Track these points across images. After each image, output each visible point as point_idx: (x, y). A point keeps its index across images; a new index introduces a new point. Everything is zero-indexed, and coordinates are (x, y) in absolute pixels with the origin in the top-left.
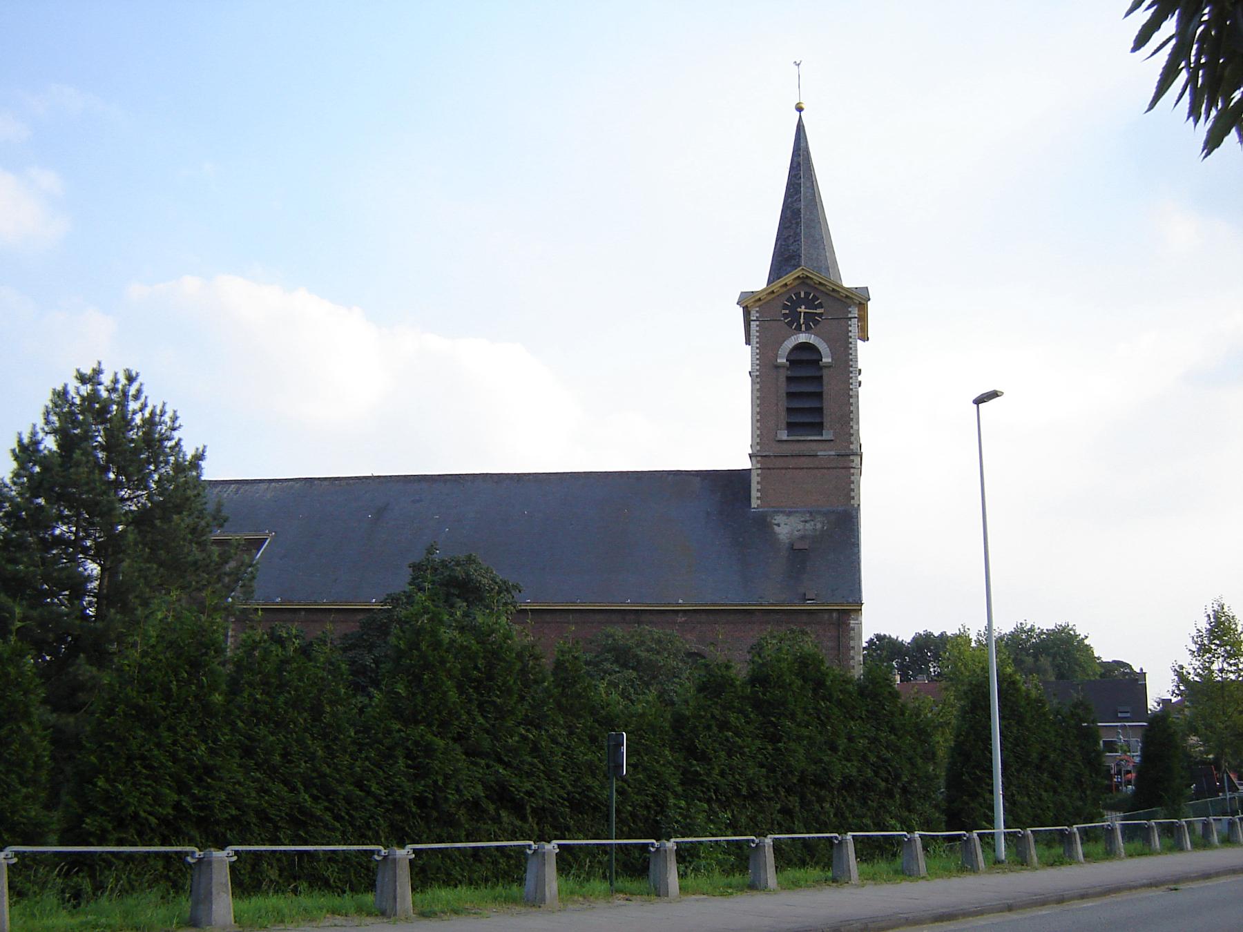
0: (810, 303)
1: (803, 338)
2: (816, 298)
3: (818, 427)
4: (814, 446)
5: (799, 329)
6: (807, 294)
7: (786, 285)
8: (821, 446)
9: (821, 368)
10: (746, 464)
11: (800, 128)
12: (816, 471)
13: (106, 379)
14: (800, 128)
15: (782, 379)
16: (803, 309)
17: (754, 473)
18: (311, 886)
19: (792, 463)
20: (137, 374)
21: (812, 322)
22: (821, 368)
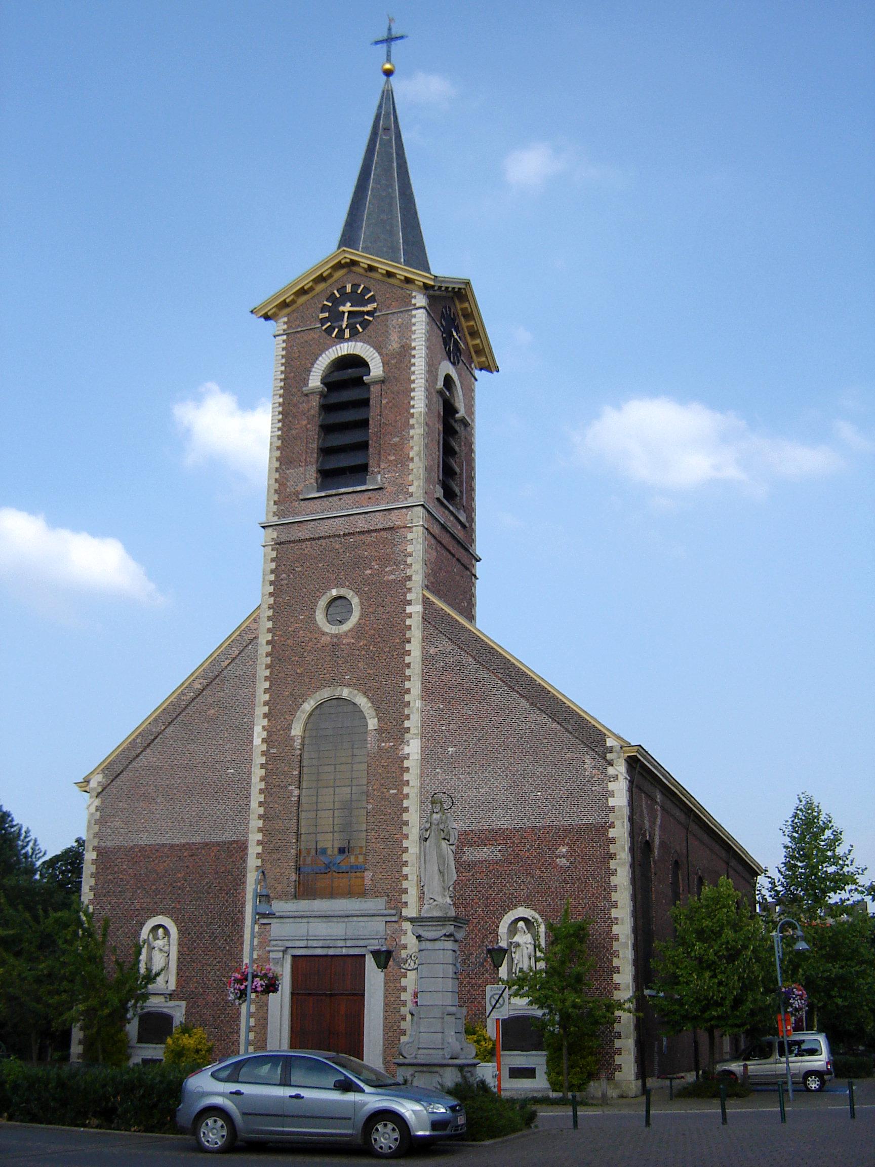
1: (345, 348)
2: (367, 290)
3: (361, 471)
6: (355, 286)
16: (347, 308)
21: (359, 325)
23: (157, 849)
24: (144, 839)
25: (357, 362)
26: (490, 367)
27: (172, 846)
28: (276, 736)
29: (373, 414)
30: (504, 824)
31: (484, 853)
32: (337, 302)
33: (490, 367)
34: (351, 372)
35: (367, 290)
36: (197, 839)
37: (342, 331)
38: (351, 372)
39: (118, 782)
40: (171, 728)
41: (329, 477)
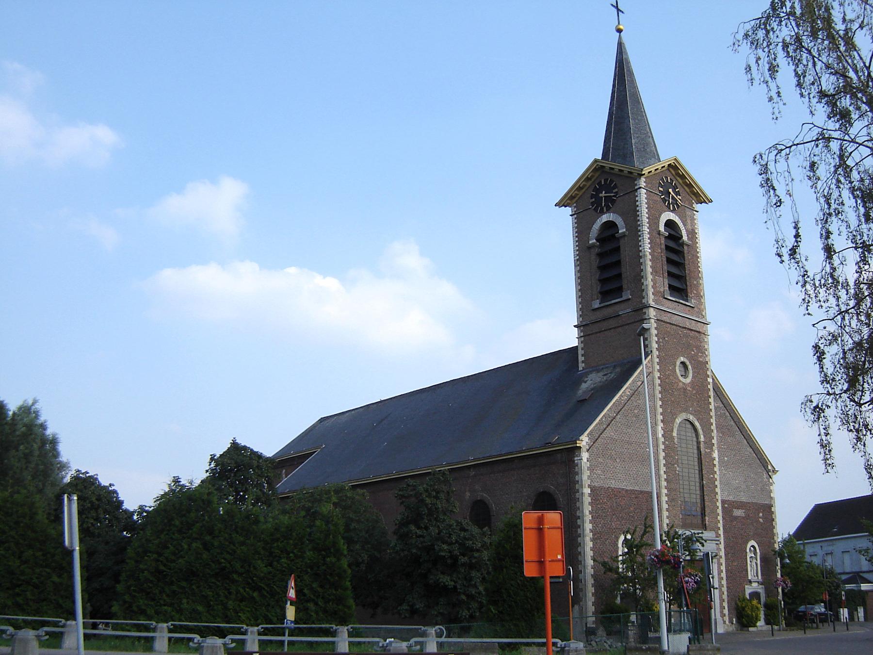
0: (608, 188)
1: (605, 218)
2: (612, 181)
3: (619, 290)
4: (617, 308)
5: (602, 212)
6: (606, 180)
7: (613, 169)
8: (622, 306)
9: (618, 239)
10: (574, 343)
11: (620, 45)
12: (620, 329)
13: (113, 488)
14: (620, 45)
15: (593, 257)
16: (603, 194)
17: (580, 349)
18: (641, 257)
19: (604, 325)
20: (561, 204)
21: (609, 205)
22: (618, 239)
23: (620, 491)
24: (613, 484)
25: (610, 225)
26: (700, 198)
27: (627, 490)
28: (667, 435)
29: (598, 288)
30: (744, 499)
31: (738, 513)
32: (598, 191)
33: (700, 198)
34: (610, 232)
35: (612, 181)
36: (637, 488)
37: (602, 209)
38: (610, 232)
39: (596, 445)
40: (619, 416)
41: (605, 295)
